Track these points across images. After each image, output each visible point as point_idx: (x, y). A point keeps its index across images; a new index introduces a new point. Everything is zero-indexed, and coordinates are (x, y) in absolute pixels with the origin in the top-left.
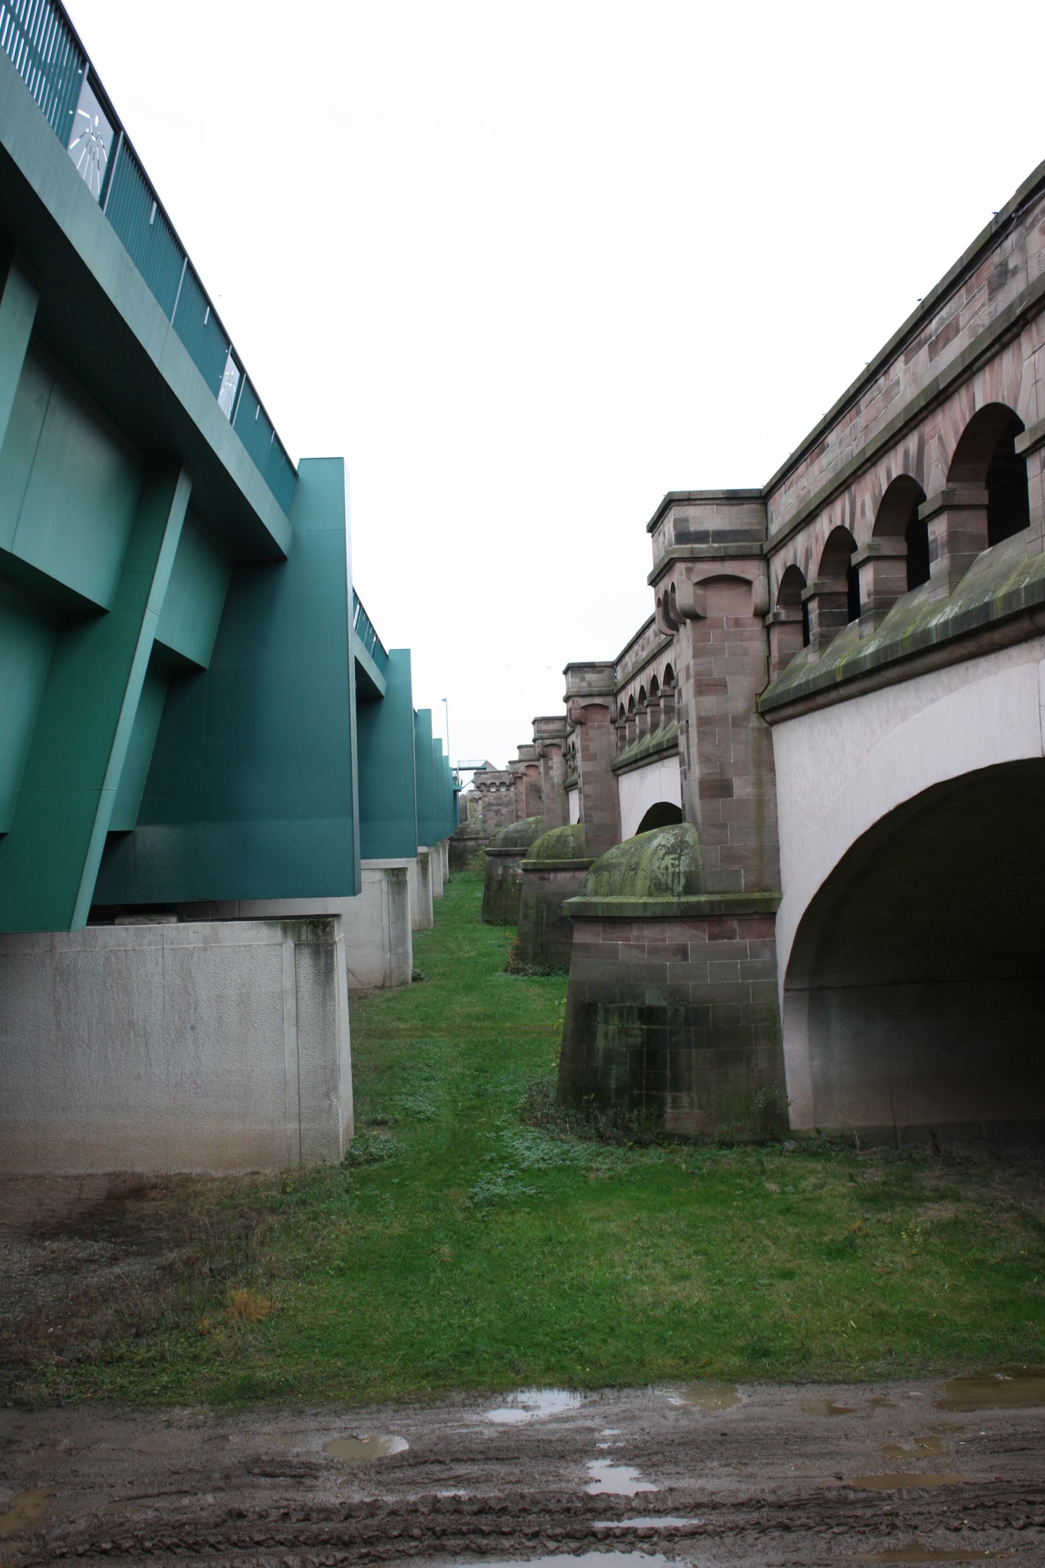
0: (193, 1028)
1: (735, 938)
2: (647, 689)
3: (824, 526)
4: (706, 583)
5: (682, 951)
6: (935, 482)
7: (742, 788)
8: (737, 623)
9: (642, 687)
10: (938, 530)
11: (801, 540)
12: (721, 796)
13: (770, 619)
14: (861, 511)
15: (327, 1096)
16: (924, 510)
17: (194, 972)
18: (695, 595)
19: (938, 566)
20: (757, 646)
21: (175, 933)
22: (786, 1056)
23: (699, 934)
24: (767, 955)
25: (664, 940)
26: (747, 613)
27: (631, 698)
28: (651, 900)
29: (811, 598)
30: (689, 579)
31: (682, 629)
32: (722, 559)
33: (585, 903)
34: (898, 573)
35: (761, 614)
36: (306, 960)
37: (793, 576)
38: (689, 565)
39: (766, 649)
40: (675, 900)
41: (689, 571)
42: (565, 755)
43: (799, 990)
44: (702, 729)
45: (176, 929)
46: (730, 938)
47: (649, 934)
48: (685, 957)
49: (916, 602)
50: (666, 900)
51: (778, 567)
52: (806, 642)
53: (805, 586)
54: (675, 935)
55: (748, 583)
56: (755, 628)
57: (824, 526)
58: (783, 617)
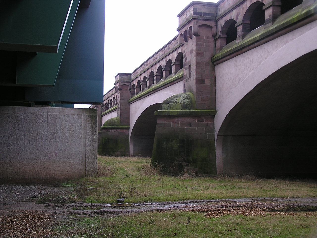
0: (56, 137)
1: (204, 122)
2: (107, 102)
3: (150, 71)
4: (200, 26)
5: (190, 124)
6: (174, 61)
7: (207, 82)
8: (208, 38)
9: (111, 99)
10: (155, 78)
11: (135, 81)
12: (201, 84)
13: (131, 90)
14: (163, 63)
15: (94, 158)
16: (172, 64)
17: (56, 121)
18: (198, 29)
19: (155, 81)
20: (212, 45)
21: (51, 110)
22: (216, 154)
23: (194, 120)
24: (212, 127)
25: (185, 121)
26: (210, 35)
27: (114, 97)
28: (181, 110)
29: (141, 85)
30: (197, 25)
31: (190, 41)
32: (205, 20)
33: (162, 111)
34: (159, 77)
35: (214, 36)
36: (89, 121)
37: (152, 73)
38: (197, 21)
39: (215, 45)
40: (189, 110)
41: (197, 22)
42: (102, 107)
43: (221, 136)
44: (197, 65)
45: (52, 109)
46: (202, 122)
47: (181, 120)
48: (191, 126)
49: (276, 25)
50: (187, 110)
51: (132, 84)
52: (146, 87)
53: (162, 69)
54: (188, 120)
55: (211, 27)
56: (212, 40)
57: (150, 71)
58: (222, 36)
